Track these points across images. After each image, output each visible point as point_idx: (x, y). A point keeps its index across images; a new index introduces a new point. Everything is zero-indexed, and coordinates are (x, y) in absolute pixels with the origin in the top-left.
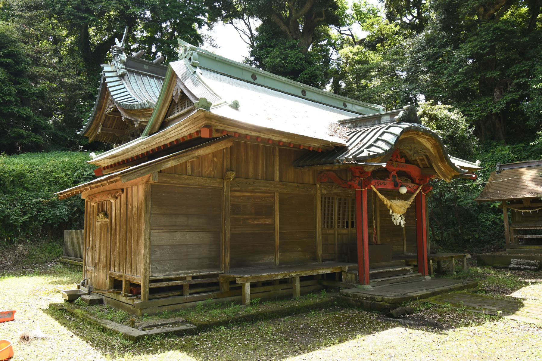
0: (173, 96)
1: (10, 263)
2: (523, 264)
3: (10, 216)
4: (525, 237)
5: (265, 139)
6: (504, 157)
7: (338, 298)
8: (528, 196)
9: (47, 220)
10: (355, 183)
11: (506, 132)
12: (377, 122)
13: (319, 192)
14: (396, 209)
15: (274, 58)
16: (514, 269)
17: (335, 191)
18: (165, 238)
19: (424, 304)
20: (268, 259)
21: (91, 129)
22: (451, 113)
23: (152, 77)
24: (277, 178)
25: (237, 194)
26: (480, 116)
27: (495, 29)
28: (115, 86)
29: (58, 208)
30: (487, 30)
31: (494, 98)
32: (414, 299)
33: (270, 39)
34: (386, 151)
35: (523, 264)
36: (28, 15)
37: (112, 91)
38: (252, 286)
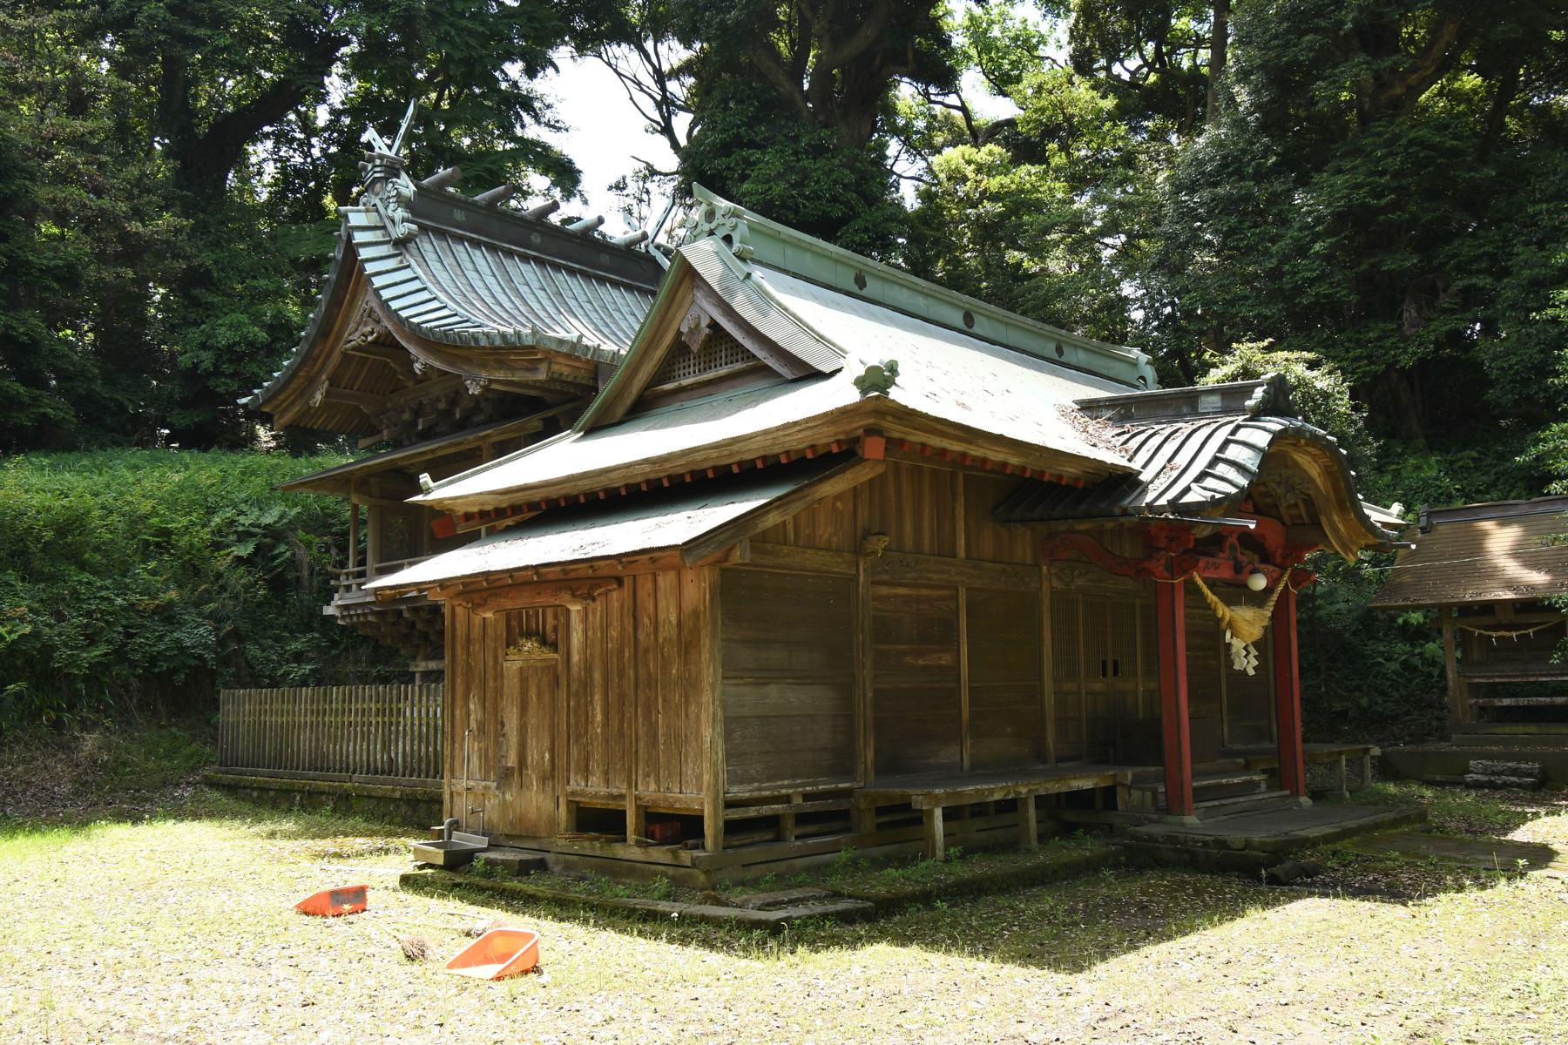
0: (679, 333)
1: (66, 788)
2: (1501, 773)
3: (54, 648)
4: (1497, 702)
5: (974, 458)
6: (1426, 484)
7: (1126, 846)
8: (1510, 595)
9: (153, 660)
10: (1158, 565)
11: (1447, 419)
12: (1185, 410)
13: (1046, 585)
14: (1244, 628)
15: (768, 181)
16: (1478, 785)
17: (1080, 582)
18: (750, 697)
19: (1334, 853)
20: (948, 754)
21: (289, 391)
22: (1315, 373)
23: (476, 244)
24: (962, 553)
25: (884, 590)
26: (1365, 374)
27: (1412, 142)
28: (388, 272)
29: (182, 625)
30: (1391, 143)
31: (1400, 326)
32: (1313, 843)
33: (752, 122)
34: (1242, 489)
35: (1501, 773)
36: (25, 23)
37: (384, 288)
38: (947, 817)
